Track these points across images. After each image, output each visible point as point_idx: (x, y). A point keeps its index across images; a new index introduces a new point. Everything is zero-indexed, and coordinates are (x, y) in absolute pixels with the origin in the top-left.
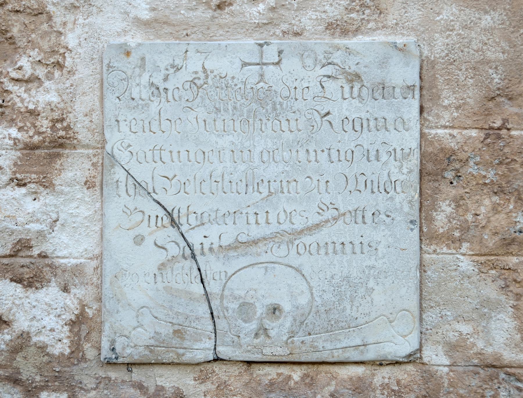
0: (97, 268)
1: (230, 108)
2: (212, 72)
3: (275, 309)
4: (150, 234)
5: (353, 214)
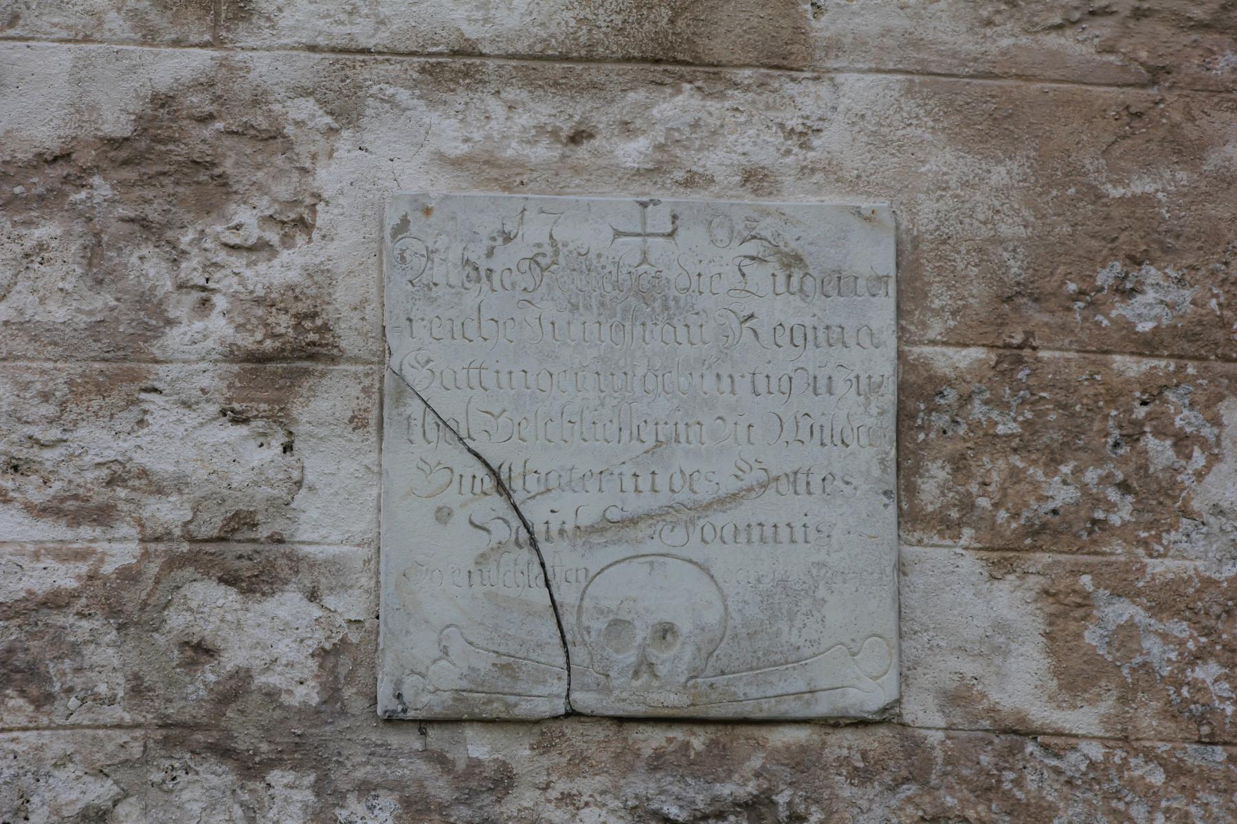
0: (369, 561)
1: (594, 303)
2: (565, 245)
3: (665, 631)
4: (463, 505)
5: (791, 479)
